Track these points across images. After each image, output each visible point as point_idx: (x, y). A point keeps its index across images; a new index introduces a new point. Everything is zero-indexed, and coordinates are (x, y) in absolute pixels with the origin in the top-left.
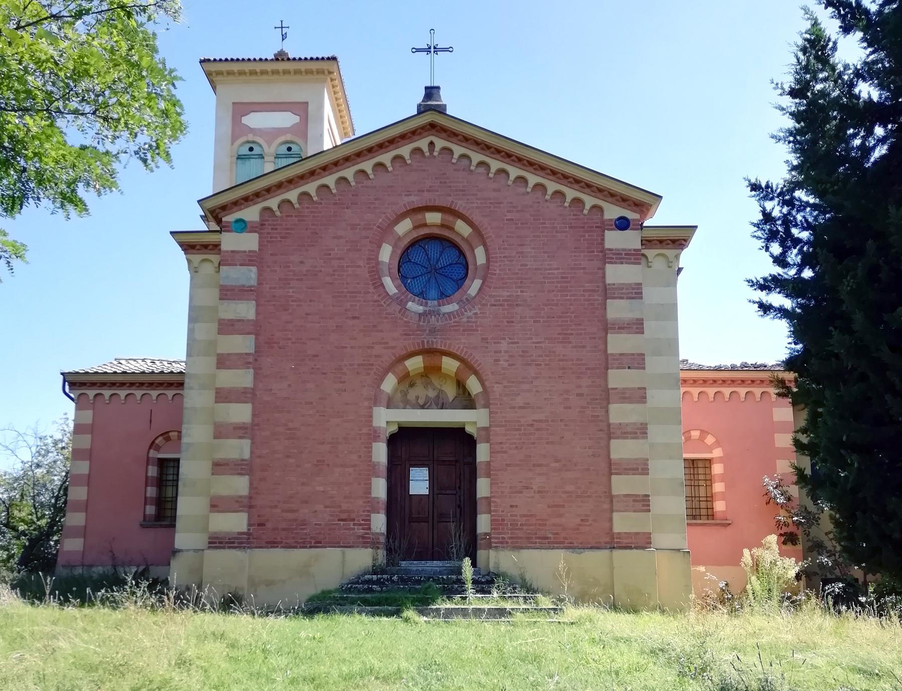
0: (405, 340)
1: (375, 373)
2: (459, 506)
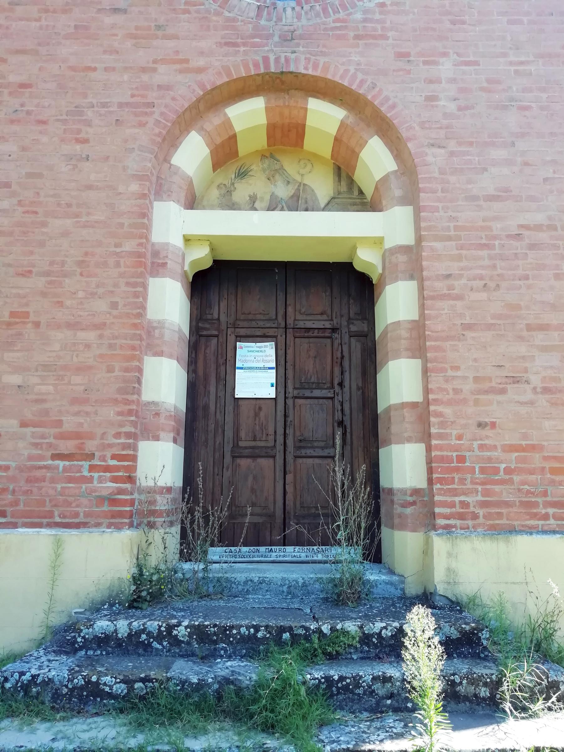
0: (226, 55)
1: (157, 122)
2: (341, 423)
